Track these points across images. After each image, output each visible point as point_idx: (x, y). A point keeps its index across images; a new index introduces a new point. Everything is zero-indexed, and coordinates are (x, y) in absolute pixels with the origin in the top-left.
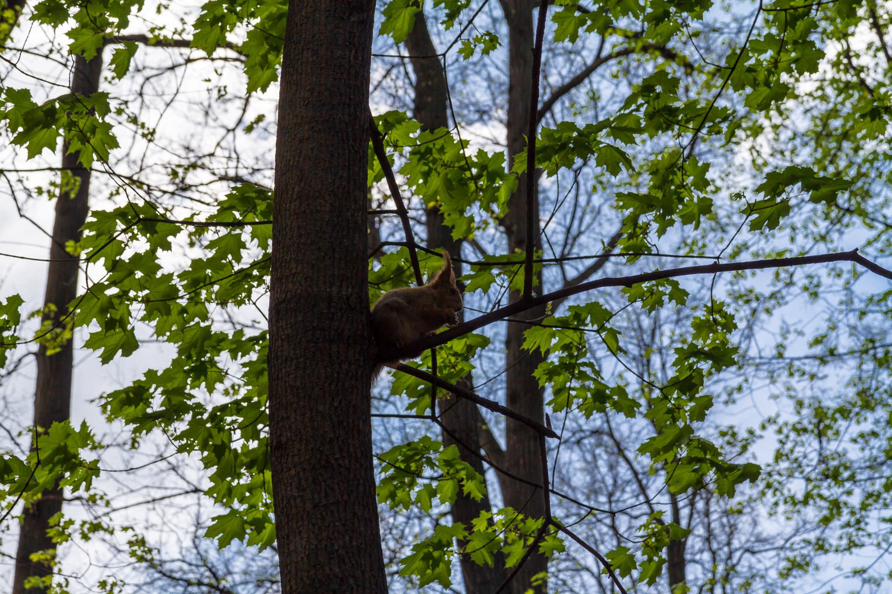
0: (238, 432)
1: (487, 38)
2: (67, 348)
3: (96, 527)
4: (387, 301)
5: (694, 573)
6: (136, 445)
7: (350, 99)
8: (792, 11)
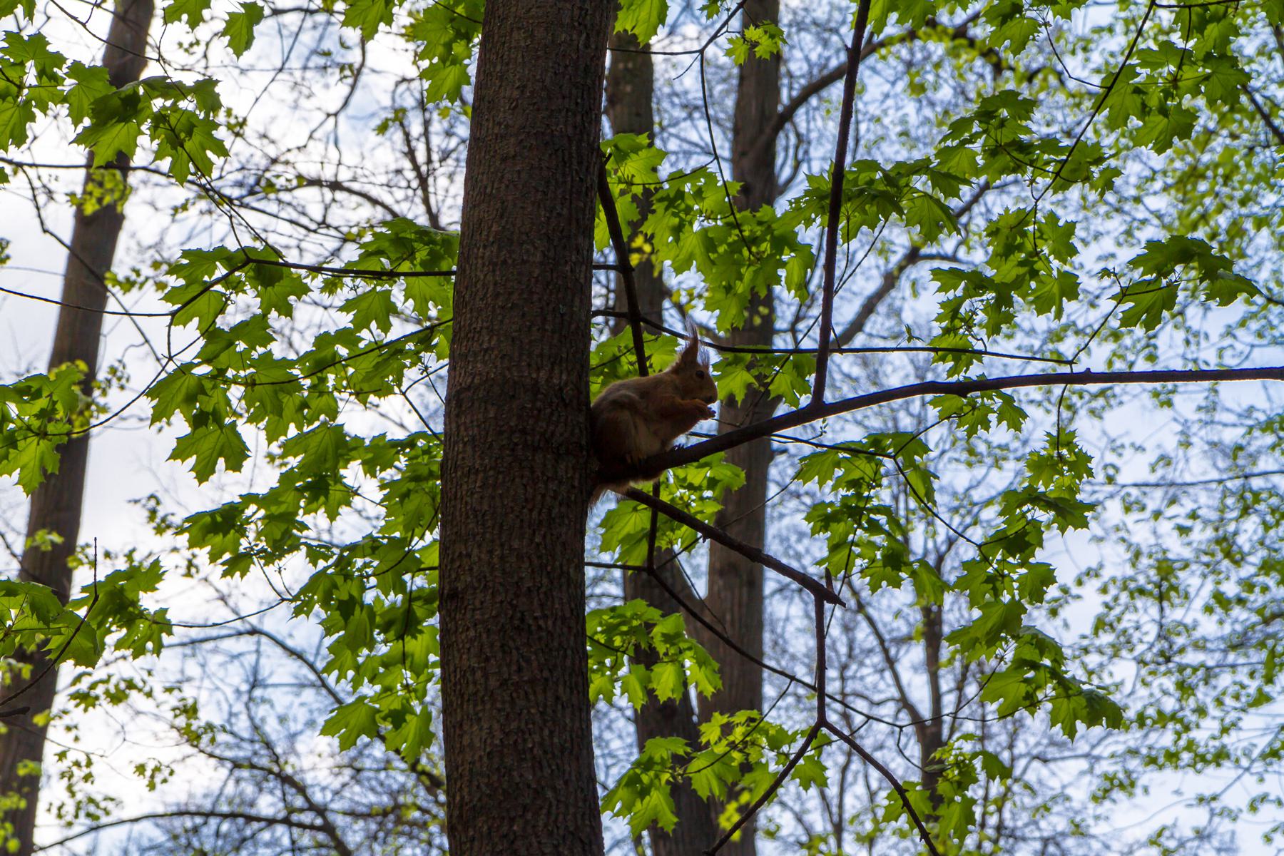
7: (577, 104)
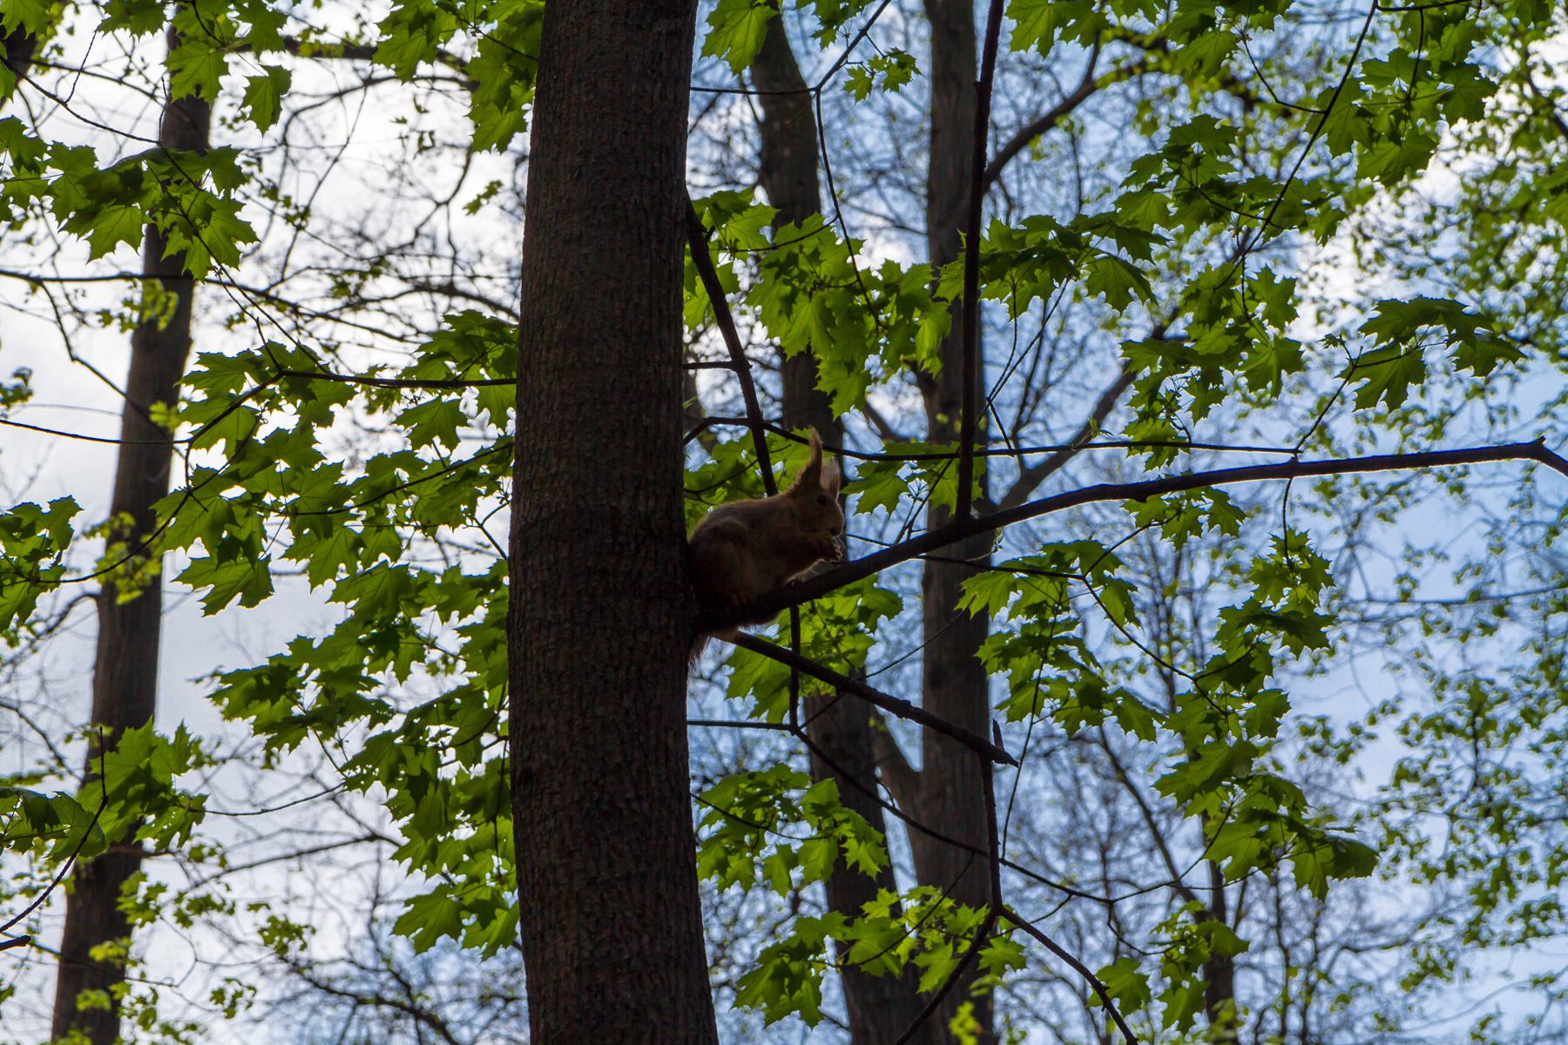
0: (451, 752)
1: (894, 61)
2: (153, 590)
3: (203, 905)
4: (714, 524)
5: (1249, 986)
6: (274, 760)
7: (653, 169)
8: (1435, 10)
